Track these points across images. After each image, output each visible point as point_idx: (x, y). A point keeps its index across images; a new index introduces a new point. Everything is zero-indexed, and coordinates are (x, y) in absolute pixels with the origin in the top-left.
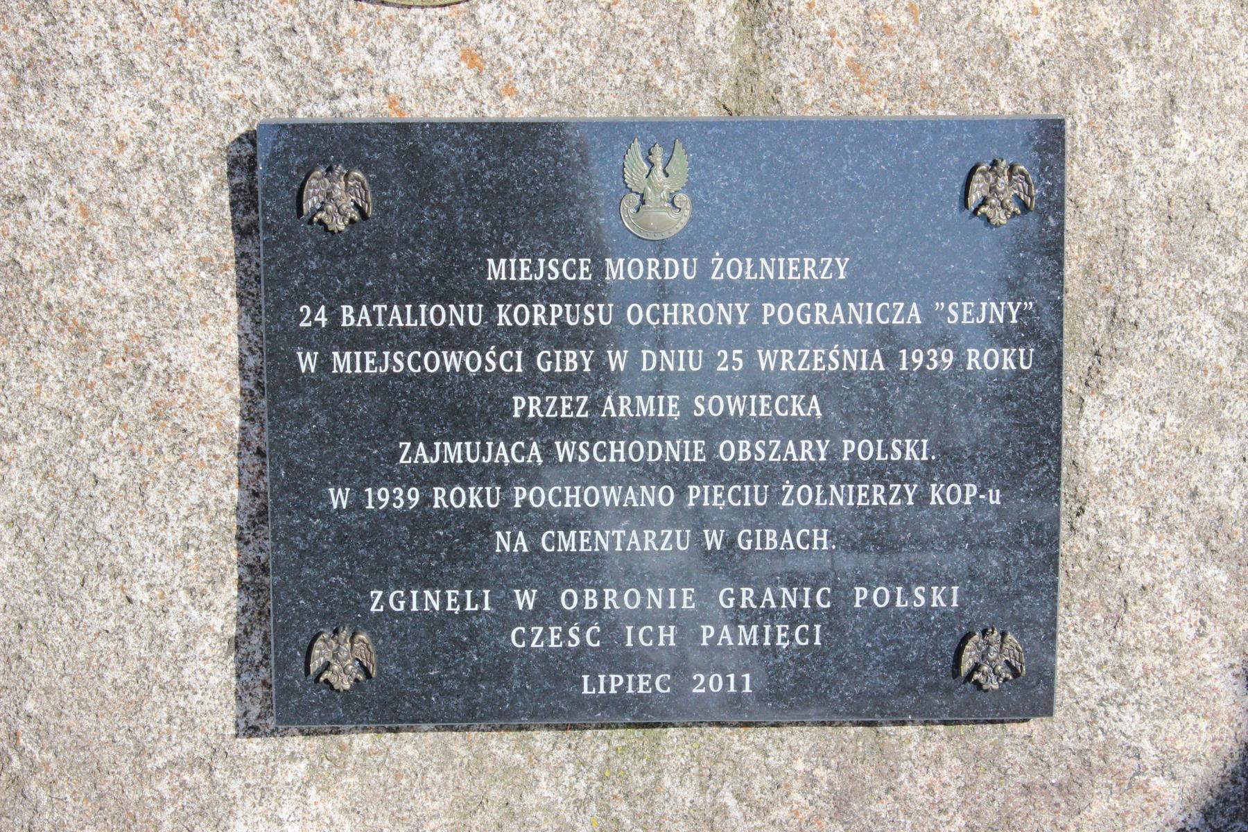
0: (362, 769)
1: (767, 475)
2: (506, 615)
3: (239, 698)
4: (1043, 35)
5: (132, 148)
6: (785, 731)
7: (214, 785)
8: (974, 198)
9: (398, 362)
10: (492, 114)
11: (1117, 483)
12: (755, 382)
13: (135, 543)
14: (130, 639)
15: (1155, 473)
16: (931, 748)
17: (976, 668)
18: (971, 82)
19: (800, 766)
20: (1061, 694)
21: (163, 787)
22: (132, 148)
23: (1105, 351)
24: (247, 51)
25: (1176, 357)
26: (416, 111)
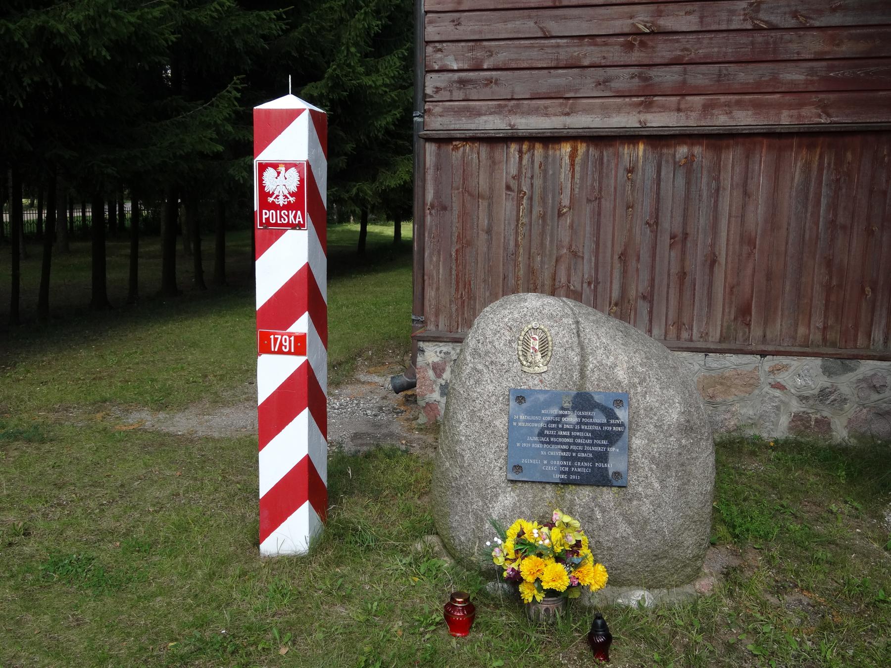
1: (582, 445)
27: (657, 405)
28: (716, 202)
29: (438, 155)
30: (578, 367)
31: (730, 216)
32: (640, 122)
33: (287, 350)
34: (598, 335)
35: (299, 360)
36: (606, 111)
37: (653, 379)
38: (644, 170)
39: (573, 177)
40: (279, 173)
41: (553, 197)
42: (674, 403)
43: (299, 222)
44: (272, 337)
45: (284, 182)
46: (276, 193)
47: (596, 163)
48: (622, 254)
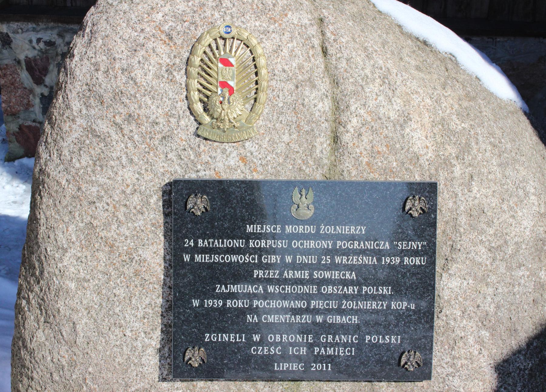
2: (250, 343)
3: (160, 369)
4: (430, 155)
5: (131, 187)
6: (342, 383)
9: (217, 258)
11: (453, 302)
13: (127, 316)
14: (125, 348)
17: (406, 363)
20: (434, 372)
22: (131, 187)
23: (449, 259)
24: (170, 156)
25: (473, 261)
27: (494, 202)
30: (326, 125)
34: (366, 49)
42: (527, 194)
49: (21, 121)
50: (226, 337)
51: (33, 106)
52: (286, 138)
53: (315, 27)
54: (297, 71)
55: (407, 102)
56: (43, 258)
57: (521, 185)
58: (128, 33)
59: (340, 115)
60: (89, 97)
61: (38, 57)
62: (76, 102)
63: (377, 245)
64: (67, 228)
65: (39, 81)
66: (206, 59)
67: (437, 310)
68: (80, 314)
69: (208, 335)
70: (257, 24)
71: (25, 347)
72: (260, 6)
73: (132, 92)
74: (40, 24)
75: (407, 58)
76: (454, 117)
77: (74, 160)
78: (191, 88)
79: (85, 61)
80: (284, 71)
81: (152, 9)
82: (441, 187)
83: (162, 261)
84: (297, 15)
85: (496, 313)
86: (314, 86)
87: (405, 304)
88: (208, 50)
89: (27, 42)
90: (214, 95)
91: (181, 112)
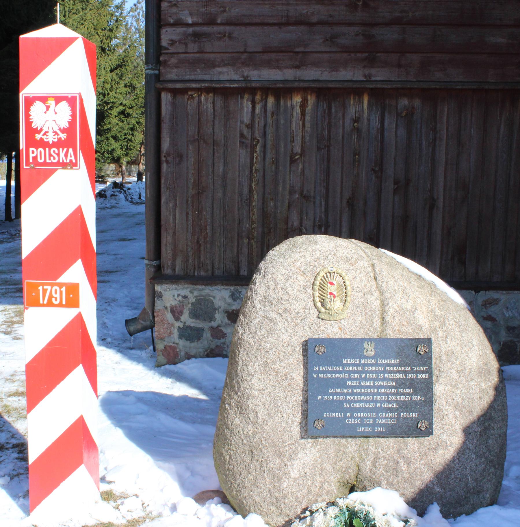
0: (320, 445)
2: (346, 417)
3: (300, 433)
4: (427, 326)
5: (287, 343)
6: (389, 439)
7: (295, 448)
8: (315, 425)
9: (329, 376)
10: (343, 337)
11: (441, 397)
12: (384, 379)
13: (284, 407)
14: (283, 423)
15: (447, 396)
16: (413, 442)
17: (421, 427)
18: (416, 333)
19: (392, 444)
20: (434, 432)
21: (287, 448)
22: (287, 343)
23: (439, 376)
24: (305, 328)
25: (450, 377)
26: (332, 337)
27: (458, 348)
28: (434, 150)
29: (174, 104)
30: (378, 312)
31: (446, 162)
32: (365, 76)
33: (57, 302)
34: (394, 278)
35: (71, 313)
36: (334, 65)
37: (451, 322)
38: (369, 120)
39: (304, 126)
40: (48, 108)
41: (286, 146)
42: (473, 345)
43: (71, 161)
44: (40, 288)
45: (55, 117)
46: (45, 129)
47: (324, 113)
48: (350, 198)
49: (165, 343)
50: (334, 415)
51: (173, 334)
52: (360, 318)
53: (371, 268)
54: (364, 288)
55: (415, 302)
56: (240, 381)
57: (470, 341)
58: (284, 271)
59: (384, 308)
60: (265, 302)
61: (178, 305)
62: (259, 304)
63: (405, 368)
64: (254, 364)
65: (177, 319)
66: (322, 282)
67: (434, 401)
68: (260, 407)
69: (325, 414)
70: (345, 266)
71: (227, 428)
72: (345, 258)
73: (287, 299)
74: (180, 285)
75: (413, 282)
76: (437, 309)
77: (258, 332)
78: (315, 295)
79: (263, 285)
80: (358, 287)
81: (295, 260)
82: (433, 341)
83: (302, 378)
84: (362, 262)
85: (462, 403)
86: (372, 294)
87: (419, 397)
88: (323, 278)
89: (172, 296)
90: (326, 299)
91: (310, 307)
